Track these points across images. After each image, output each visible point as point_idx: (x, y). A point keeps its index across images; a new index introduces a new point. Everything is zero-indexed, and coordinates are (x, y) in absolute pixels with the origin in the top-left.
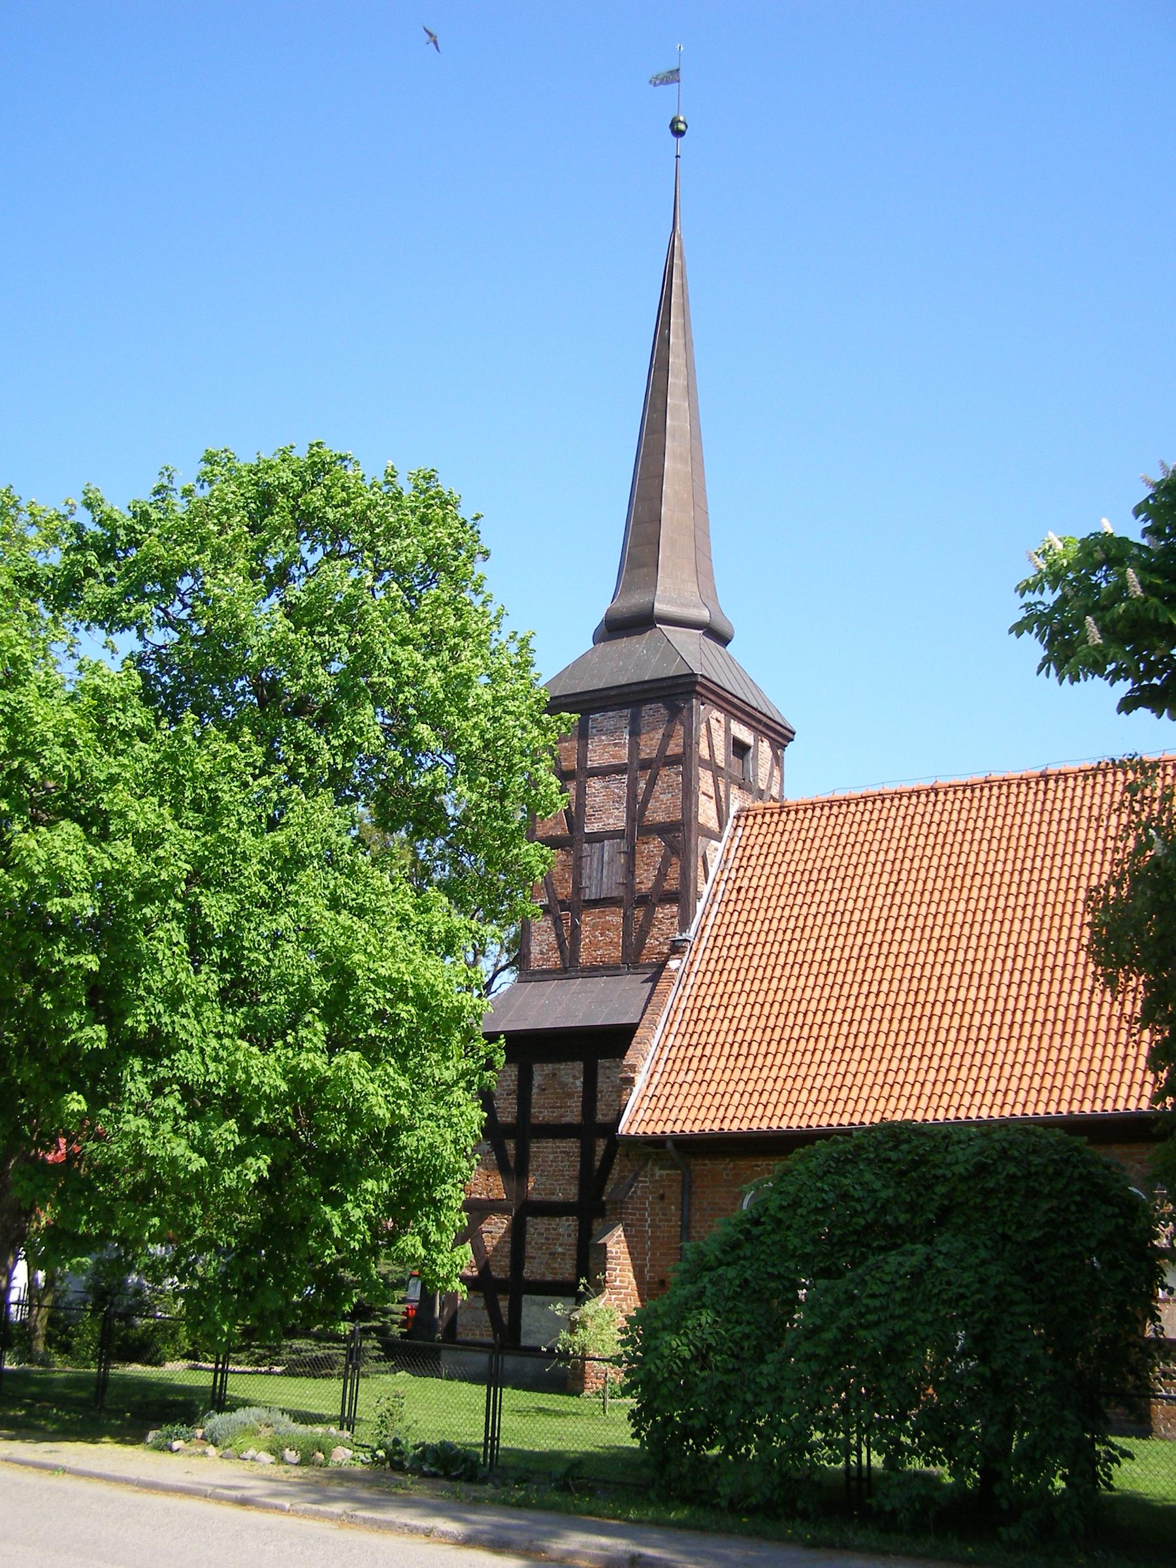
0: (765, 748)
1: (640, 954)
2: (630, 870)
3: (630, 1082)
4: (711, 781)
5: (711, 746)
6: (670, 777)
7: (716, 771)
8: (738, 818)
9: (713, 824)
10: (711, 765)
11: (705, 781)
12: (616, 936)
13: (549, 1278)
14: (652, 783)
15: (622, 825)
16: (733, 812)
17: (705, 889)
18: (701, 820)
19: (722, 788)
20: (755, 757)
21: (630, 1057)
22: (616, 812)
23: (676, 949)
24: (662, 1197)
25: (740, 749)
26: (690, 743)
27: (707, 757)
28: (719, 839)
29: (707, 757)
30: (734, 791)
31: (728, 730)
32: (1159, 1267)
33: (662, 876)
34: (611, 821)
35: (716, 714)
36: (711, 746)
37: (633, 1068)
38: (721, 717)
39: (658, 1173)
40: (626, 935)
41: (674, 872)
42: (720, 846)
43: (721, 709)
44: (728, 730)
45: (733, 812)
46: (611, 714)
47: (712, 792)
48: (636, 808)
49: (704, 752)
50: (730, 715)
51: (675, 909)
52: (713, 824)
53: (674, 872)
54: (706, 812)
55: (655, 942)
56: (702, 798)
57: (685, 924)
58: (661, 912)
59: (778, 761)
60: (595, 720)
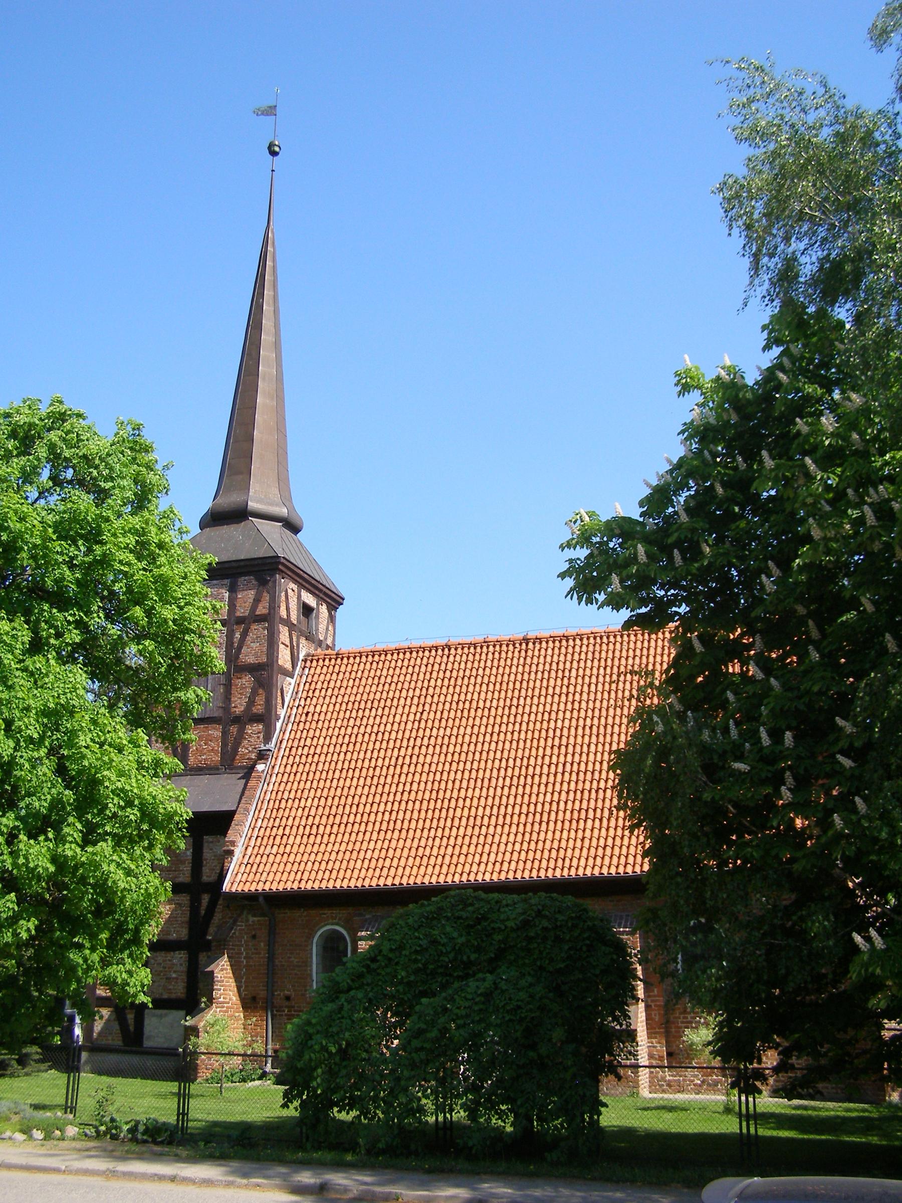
0: (324, 609)
1: (234, 759)
2: (227, 697)
3: (231, 853)
5: (288, 609)
6: (258, 631)
8: (305, 661)
9: (288, 666)
10: (287, 622)
11: (284, 634)
12: (217, 746)
13: (165, 996)
14: (244, 634)
16: (301, 657)
17: (282, 713)
18: (280, 662)
20: (317, 617)
21: (231, 835)
23: (262, 756)
24: (254, 937)
25: (307, 610)
26: (274, 606)
30: (303, 641)
31: (299, 597)
33: (251, 702)
36: (288, 609)
37: (233, 843)
39: (251, 919)
40: (224, 745)
41: (260, 700)
43: (295, 582)
44: (299, 597)
45: (301, 657)
47: (288, 642)
49: (283, 613)
50: (301, 586)
51: (261, 727)
52: (288, 666)
53: (260, 700)
54: (284, 657)
55: (246, 751)
56: (281, 646)
57: (268, 738)
58: (250, 729)
59: (332, 619)
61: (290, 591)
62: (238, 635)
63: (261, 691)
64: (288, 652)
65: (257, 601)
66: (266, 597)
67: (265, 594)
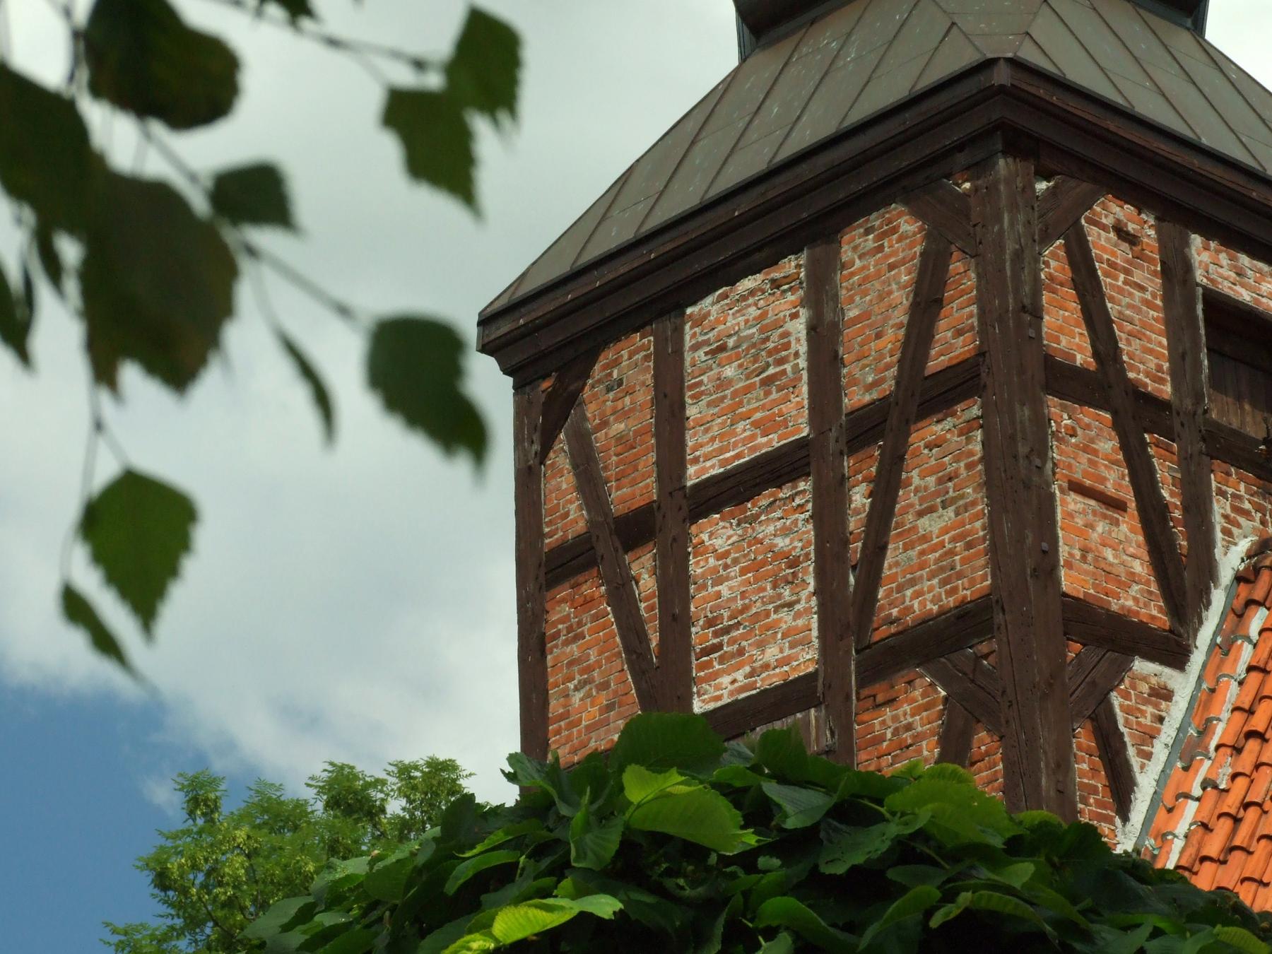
4: (1108, 445)
6: (947, 447)
7: (1137, 415)
9: (1140, 599)
10: (1103, 385)
14: (886, 489)
15: (806, 660)
16: (1230, 559)
18: (1070, 582)
19: (1165, 472)
22: (786, 617)
27: (1083, 358)
28: (1176, 656)
29: (1083, 358)
32: (511, 765)
34: (772, 654)
35: (1114, 210)
38: (1146, 227)
42: (1183, 685)
44: (1176, 272)
45: (1230, 559)
46: (747, 283)
47: (1116, 480)
48: (847, 576)
52: (1140, 599)
56: (1069, 506)
60: (698, 322)
61: (1101, 242)
62: (859, 498)
63: (982, 740)
64: (1128, 530)
65: (927, 304)
66: (963, 275)
67: (956, 266)
